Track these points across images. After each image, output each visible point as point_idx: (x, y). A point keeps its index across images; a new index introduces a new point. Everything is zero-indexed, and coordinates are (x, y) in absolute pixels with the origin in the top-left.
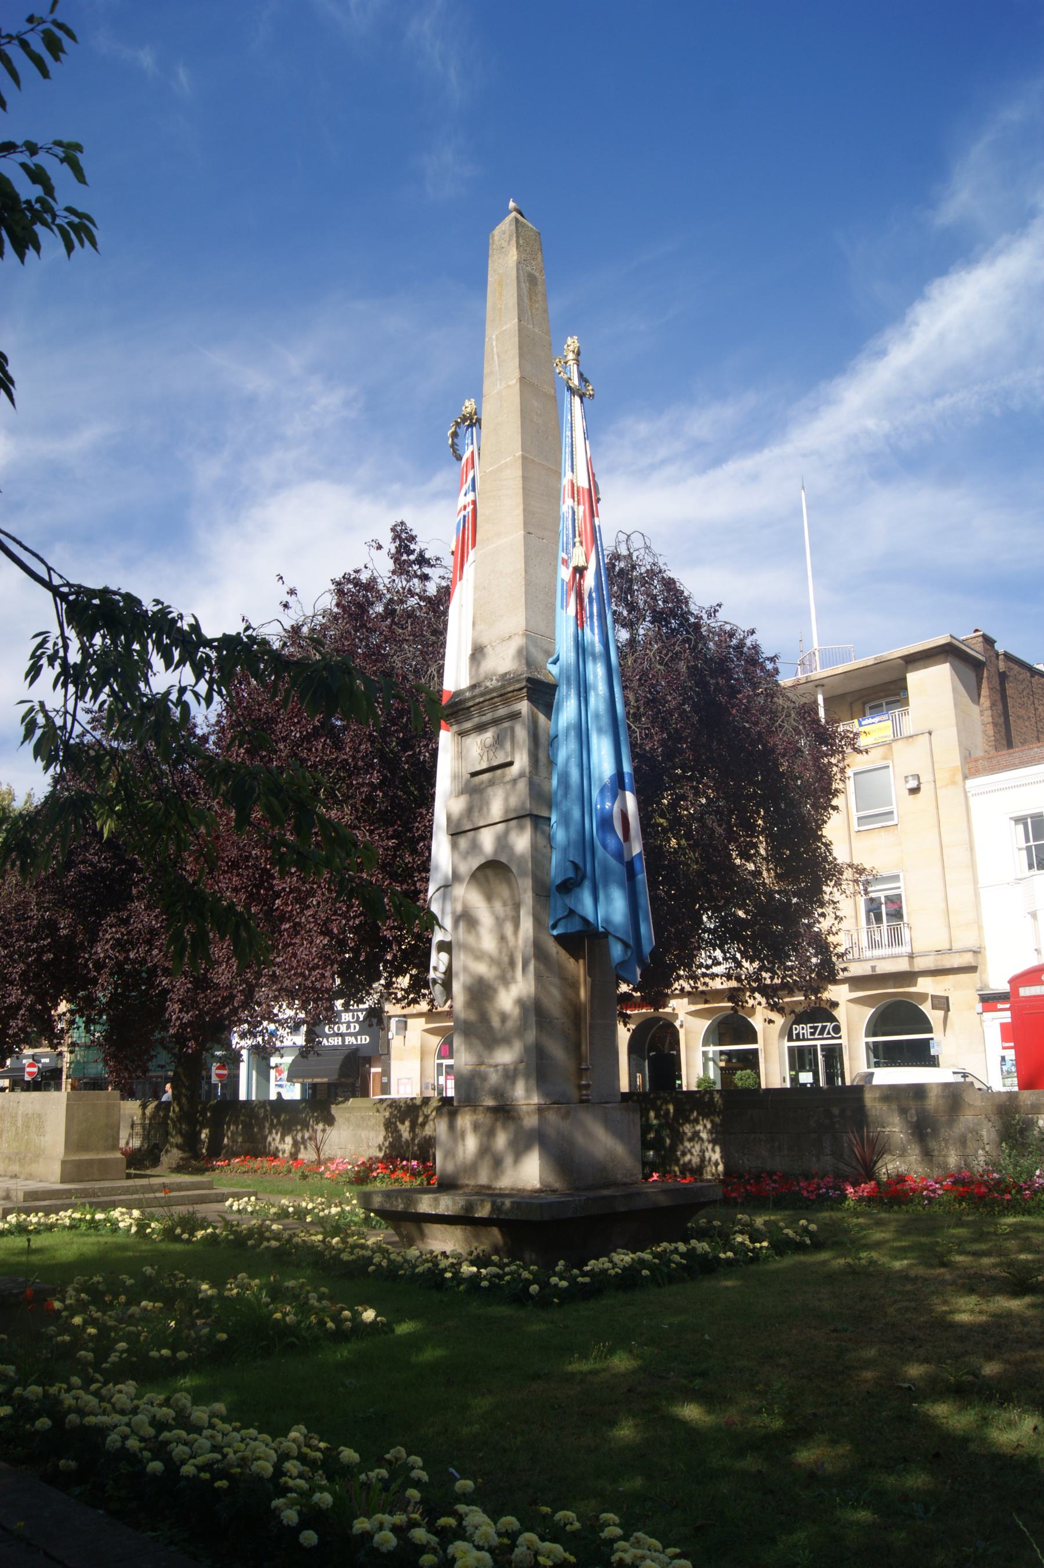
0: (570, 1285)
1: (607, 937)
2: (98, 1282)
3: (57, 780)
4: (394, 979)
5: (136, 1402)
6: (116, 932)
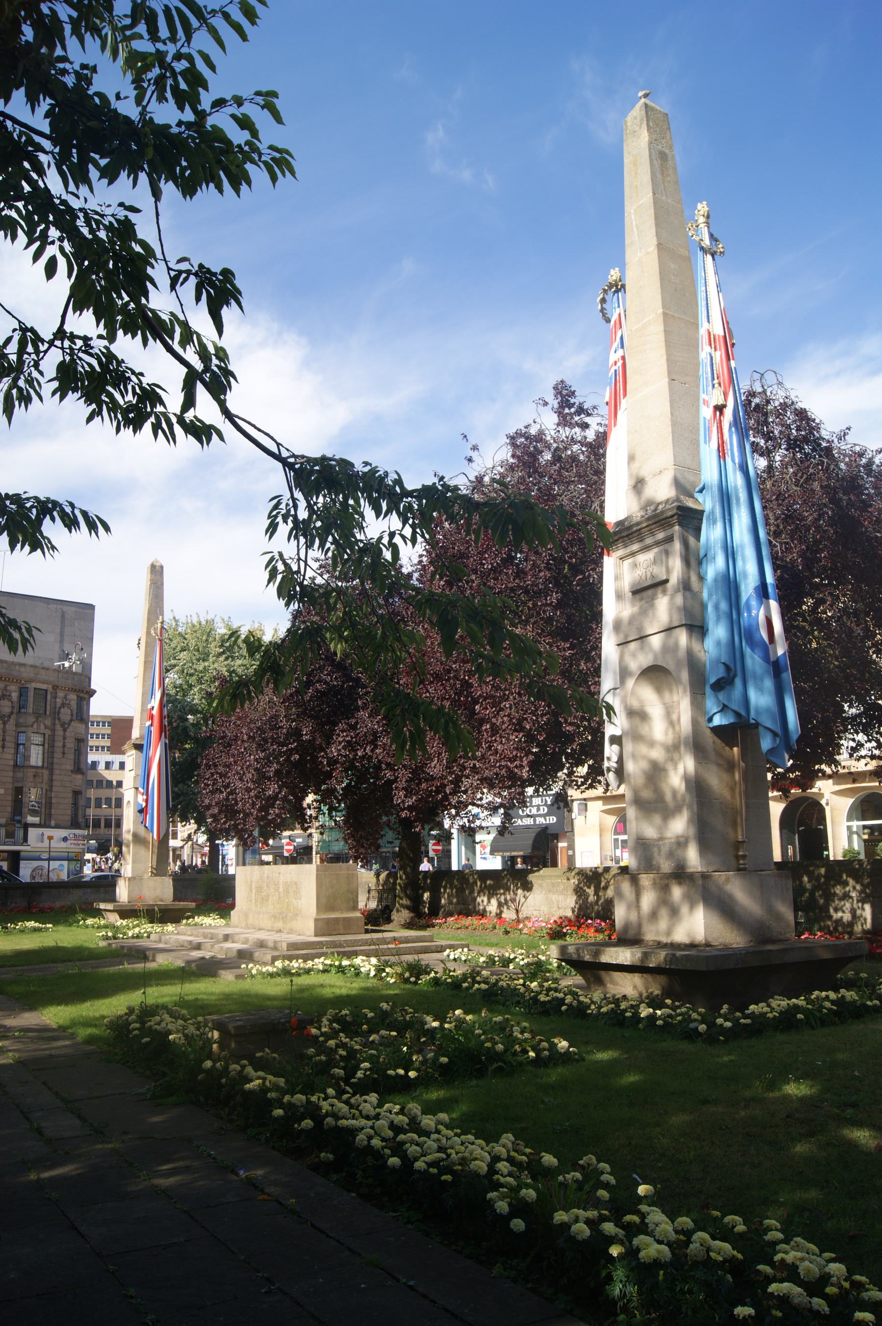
0: (733, 1026)
1: (757, 728)
2: (346, 1015)
3: (296, 616)
4: (575, 769)
5: (378, 1110)
6: (347, 736)
